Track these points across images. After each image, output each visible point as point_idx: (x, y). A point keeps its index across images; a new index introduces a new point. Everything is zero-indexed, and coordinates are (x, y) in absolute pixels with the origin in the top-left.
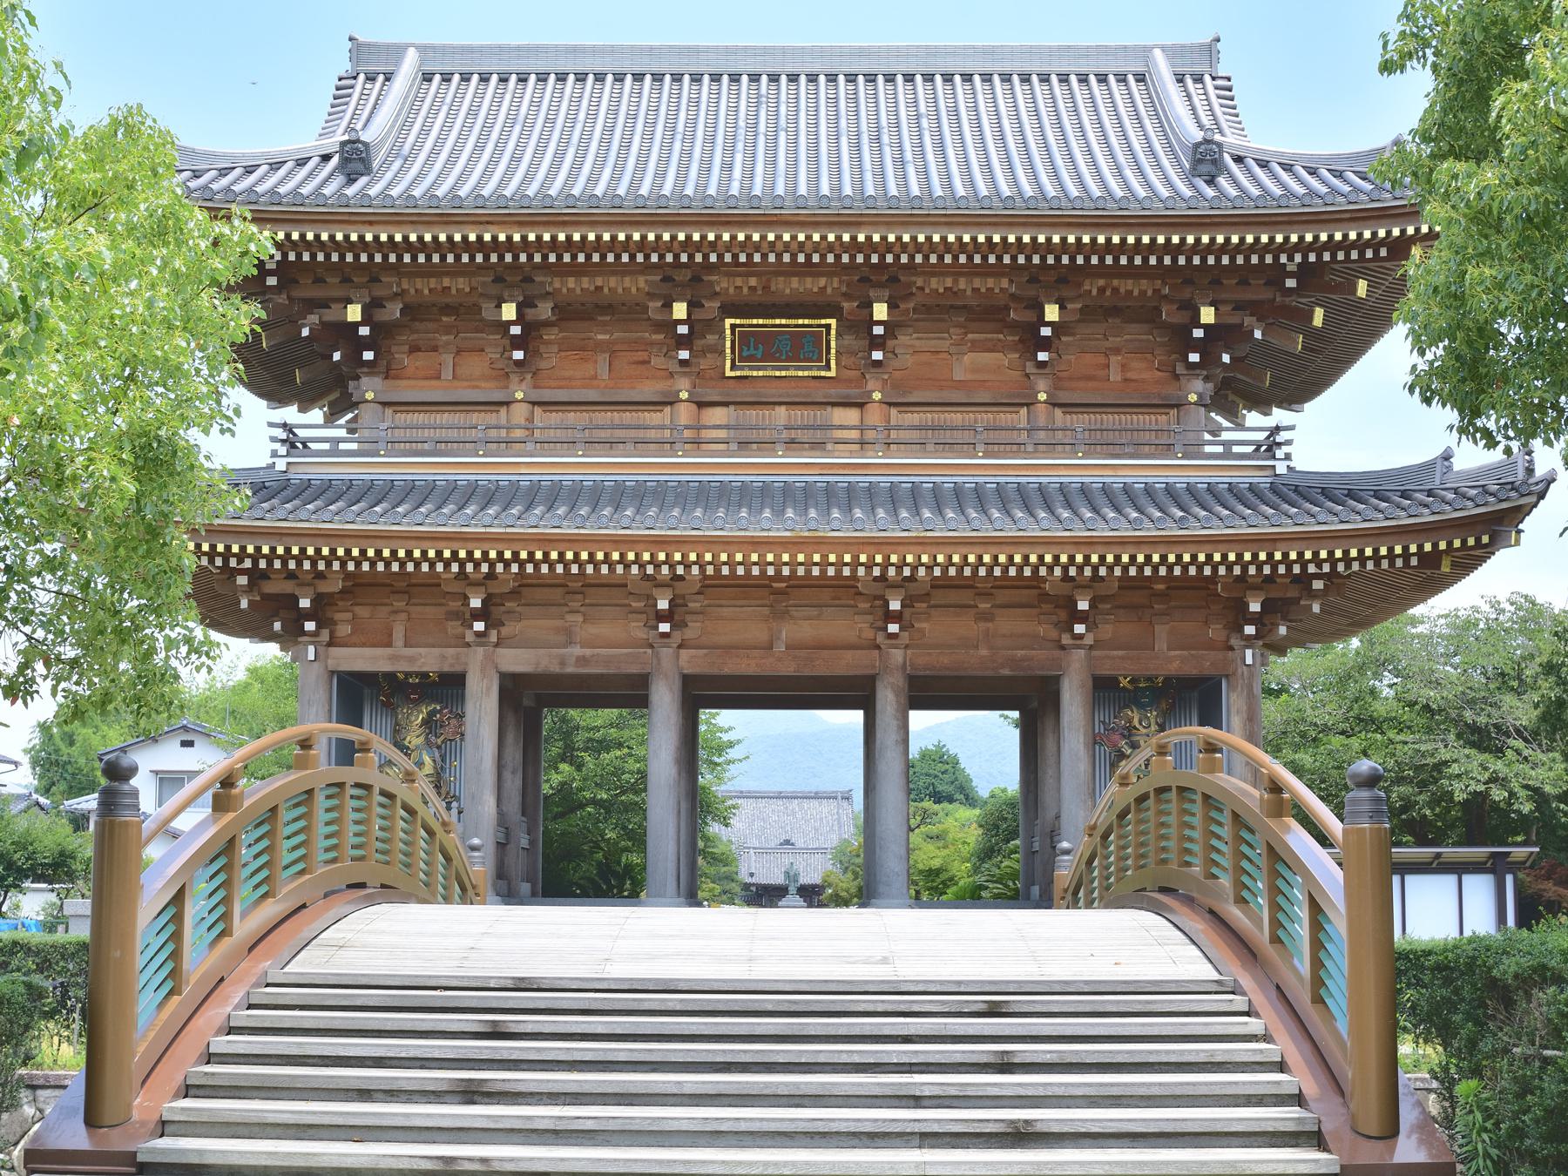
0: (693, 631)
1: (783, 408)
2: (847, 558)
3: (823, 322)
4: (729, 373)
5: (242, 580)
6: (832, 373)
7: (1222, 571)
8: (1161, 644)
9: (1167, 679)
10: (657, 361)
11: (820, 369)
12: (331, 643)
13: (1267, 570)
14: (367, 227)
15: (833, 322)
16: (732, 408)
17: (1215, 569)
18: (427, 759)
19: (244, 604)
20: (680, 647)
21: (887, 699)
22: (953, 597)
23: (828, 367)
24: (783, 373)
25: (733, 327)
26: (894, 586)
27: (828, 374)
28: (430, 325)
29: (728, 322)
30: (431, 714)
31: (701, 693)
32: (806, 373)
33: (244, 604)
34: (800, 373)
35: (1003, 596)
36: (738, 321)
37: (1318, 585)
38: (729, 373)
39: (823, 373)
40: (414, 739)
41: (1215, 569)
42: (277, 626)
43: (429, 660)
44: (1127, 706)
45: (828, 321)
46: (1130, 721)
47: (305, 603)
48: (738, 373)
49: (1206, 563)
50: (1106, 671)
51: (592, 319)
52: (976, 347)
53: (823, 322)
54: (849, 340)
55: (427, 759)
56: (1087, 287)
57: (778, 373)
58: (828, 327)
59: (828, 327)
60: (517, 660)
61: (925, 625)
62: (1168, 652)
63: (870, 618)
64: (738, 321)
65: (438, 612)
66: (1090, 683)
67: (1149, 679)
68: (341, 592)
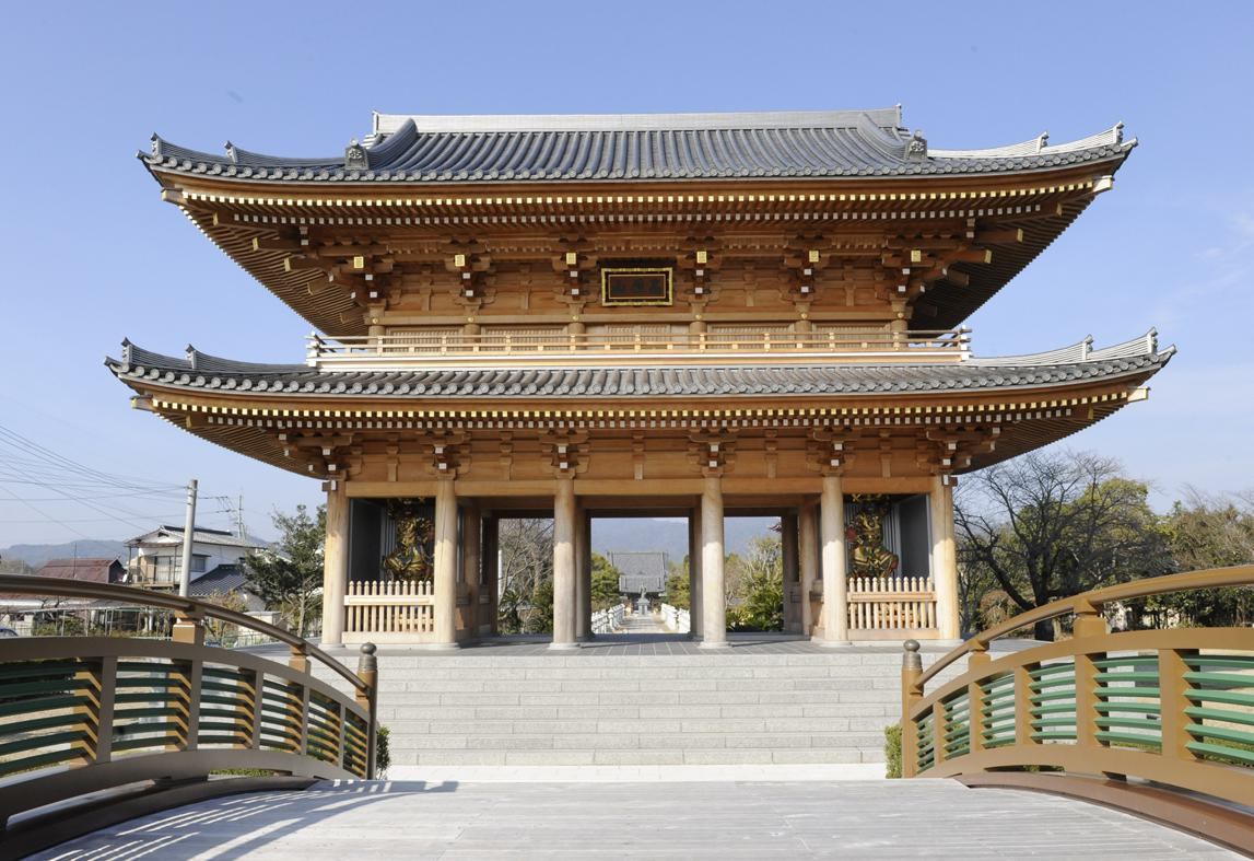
0: (582, 468)
1: (638, 328)
2: (664, 414)
3: (664, 270)
4: (670, 270)
5: (283, 437)
6: (670, 303)
7: (816, 422)
8: (886, 473)
9: (884, 495)
10: (560, 298)
11: (662, 300)
12: (348, 478)
13: (847, 422)
14: (399, 407)
15: (670, 270)
16: (606, 327)
17: (811, 422)
18: (416, 552)
19: (287, 453)
20: (574, 478)
21: (710, 513)
22: (750, 443)
23: (667, 300)
24: (639, 304)
25: (607, 274)
26: (714, 436)
27: (667, 304)
28: (415, 277)
29: (604, 270)
30: (419, 524)
31: (587, 510)
32: (654, 303)
33: (287, 453)
34: (650, 303)
35: (783, 442)
36: (610, 270)
37: (996, 431)
38: (604, 304)
39: (664, 303)
40: (407, 540)
41: (811, 422)
42: (311, 468)
43: (418, 490)
44: (859, 513)
45: (667, 269)
46: (862, 522)
47: (326, 452)
48: (610, 304)
49: (805, 417)
50: (849, 491)
51: (519, 271)
52: (761, 287)
53: (664, 270)
54: (681, 281)
55: (416, 552)
56: (834, 244)
57: (635, 304)
58: (667, 273)
59: (667, 273)
60: (470, 489)
61: (733, 462)
62: (887, 480)
63: (697, 458)
64: (610, 270)
65: (418, 457)
66: (841, 499)
67: (873, 495)
68: (352, 445)
